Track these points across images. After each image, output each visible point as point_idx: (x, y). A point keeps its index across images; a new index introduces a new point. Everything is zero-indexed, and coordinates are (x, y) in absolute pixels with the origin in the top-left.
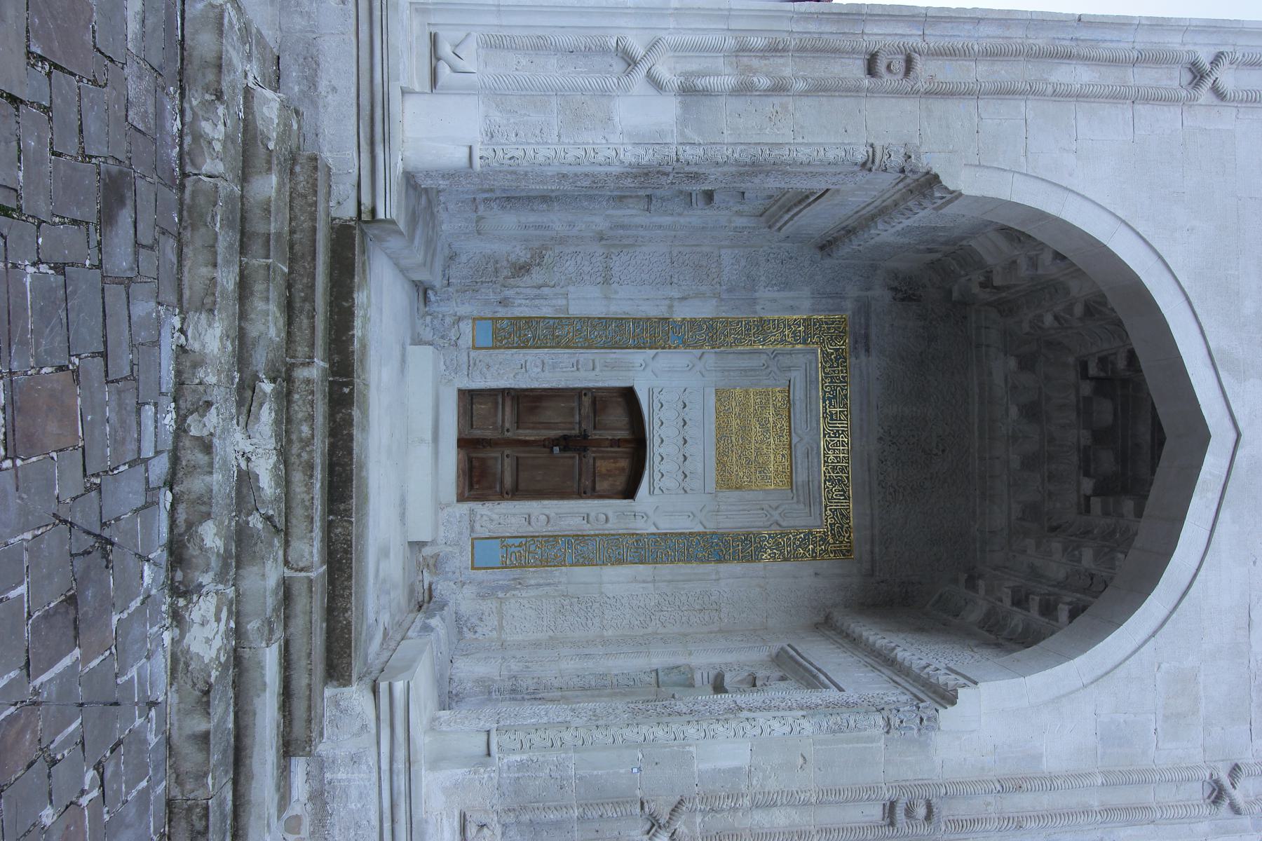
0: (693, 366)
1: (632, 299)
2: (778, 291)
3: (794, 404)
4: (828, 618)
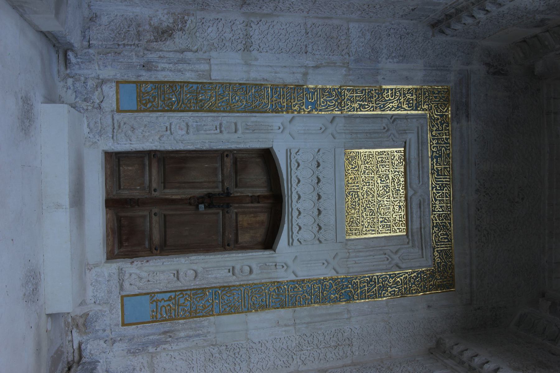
0: (326, 129)
1: (271, 66)
2: (397, 62)
3: (410, 162)
4: (439, 343)
